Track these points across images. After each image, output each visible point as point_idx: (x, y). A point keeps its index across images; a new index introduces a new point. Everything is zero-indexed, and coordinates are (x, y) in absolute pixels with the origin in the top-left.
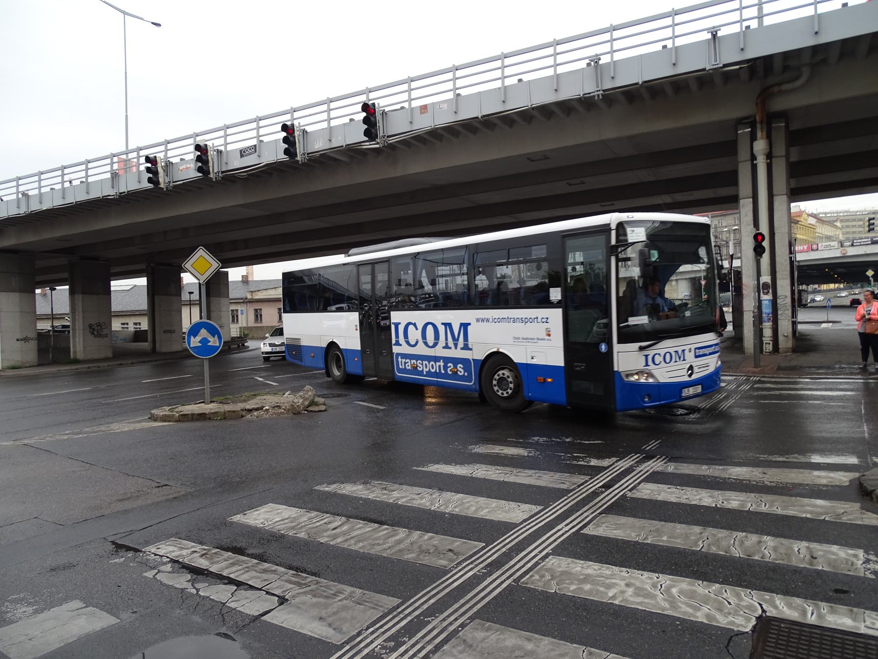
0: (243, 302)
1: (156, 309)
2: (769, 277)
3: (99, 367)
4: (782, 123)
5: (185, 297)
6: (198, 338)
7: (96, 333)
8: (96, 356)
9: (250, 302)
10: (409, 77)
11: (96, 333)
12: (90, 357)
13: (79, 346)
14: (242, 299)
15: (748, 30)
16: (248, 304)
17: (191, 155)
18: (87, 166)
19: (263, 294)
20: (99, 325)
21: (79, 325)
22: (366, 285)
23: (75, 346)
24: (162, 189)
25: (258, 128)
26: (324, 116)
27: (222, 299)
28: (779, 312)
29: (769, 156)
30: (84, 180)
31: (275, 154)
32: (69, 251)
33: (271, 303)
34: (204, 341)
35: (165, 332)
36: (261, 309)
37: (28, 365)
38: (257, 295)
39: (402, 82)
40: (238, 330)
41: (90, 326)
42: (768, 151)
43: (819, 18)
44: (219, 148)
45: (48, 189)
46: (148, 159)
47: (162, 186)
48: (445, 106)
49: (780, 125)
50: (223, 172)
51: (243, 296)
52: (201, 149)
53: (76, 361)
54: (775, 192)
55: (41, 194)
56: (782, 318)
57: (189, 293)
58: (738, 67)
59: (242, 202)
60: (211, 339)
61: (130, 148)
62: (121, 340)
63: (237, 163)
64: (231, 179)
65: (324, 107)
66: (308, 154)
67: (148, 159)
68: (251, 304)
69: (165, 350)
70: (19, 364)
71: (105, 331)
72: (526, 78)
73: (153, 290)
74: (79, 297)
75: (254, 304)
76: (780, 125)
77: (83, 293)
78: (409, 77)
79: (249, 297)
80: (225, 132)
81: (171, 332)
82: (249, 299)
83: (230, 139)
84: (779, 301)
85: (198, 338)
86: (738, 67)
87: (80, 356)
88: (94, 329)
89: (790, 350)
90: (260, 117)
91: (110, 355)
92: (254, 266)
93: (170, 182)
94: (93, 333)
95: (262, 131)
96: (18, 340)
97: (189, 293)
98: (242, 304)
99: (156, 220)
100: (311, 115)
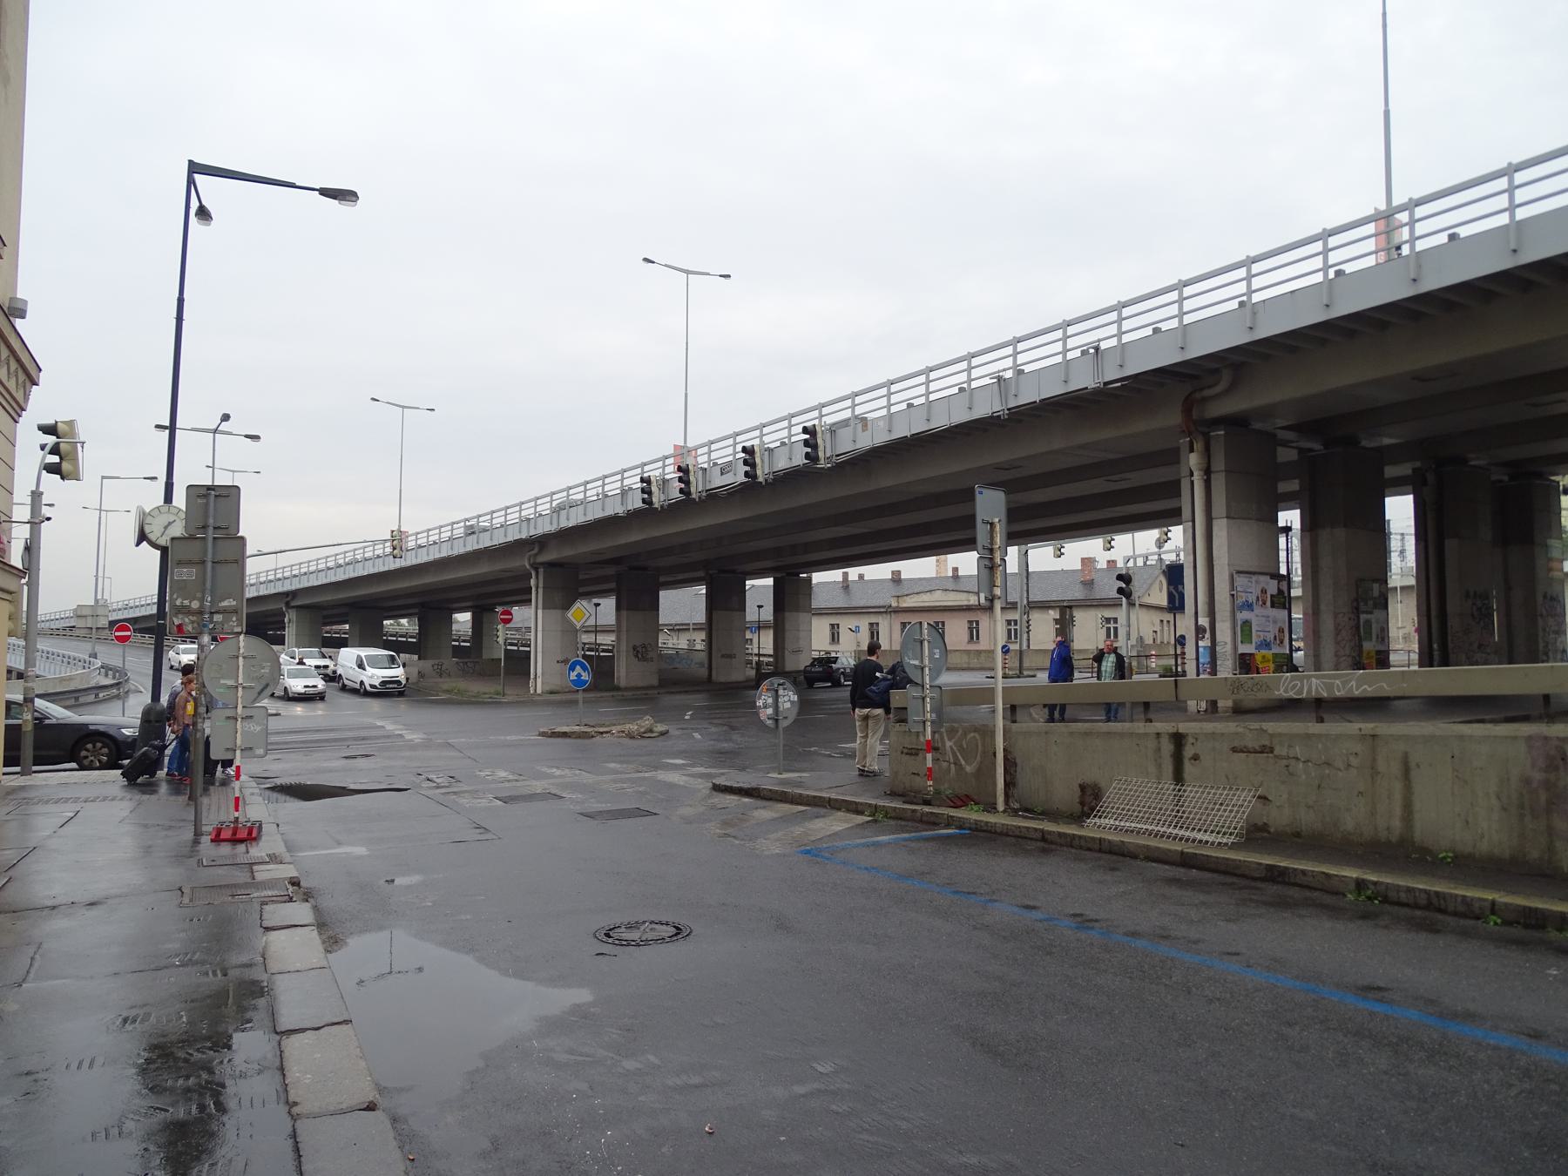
0: (886, 612)
1: (714, 627)
2: (1207, 619)
3: (623, 696)
4: (1221, 430)
5: (751, 614)
6: (575, 673)
7: (640, 656)
8: (641, 684)
9: (895, 612)
10: (1119, 302)
11: (640, 656)
12: (633, 684)
13: (624, 672)
14: (884, 607)
15: (1340, 278)
16: (892, 614)
17: (671, 473)
18: (603, 482)
19: (913, 600)
20: (644, 646)
21: (624, 647)
22: (1285, 568)
23: (619, 671)
24: (761, 483)
25: (1015, 354)
26: (1503, 201)
27: (801, 614)
28: (1218, 663)
29: (1208, 472)
30: (1244, 298)
31: (636, 502)
32: (616, 561)
33: (955, 614)
34: (579, 675)
35: (723, 656)
36: (877, 624)
37: (567, 690)
38: (905, 602)
39: (1362, 223)
40: (853, 654)
41: (635, 648)
42: (1206, 465)
43: (1519, 227)
44: (702, 466)
45: (1077, 353)
46: (744, 450)
47: (761, 479)
48: (881, 423)
49: (1219, 433)
50: (707, 491)
51: (887, 603)
52: (646, 480)
53: (618, 689)
54: (1214, 515)
55: (890, 416)
56: (1222, 669)
57: (758, 606)
58: (1119, 384)
59: (739, 517)
60: (583, 674)
61: (1395, 203)
62: (696, 664)
63: (718, 481)
64: (714, 498)
65: (1318, 246)
66: (774, 473)
67: (744, 450)
68: (897, 615)
69: (722, 679)
70: (558, 688)
71: (651, 655)
72: (1464, 232)
73: (712, 603)
74: (624, 613)
75: (900, 614)
76: (1219, 433)
77: (627, 609)
78: (1119, 302)
79: (894, 604)
80: (889, 390)
81: (731, 656)
82: (894, 608)
83: (1257, 283)
84: (1218, 648)
85: (575, 673)
86: (1119, 384)
87: (623, 684)
88: (638, 651)
89: (1230, 710)
90: (973, 353)
91: (655, 682)
92: (948, 556)
93: (665, 501)
94: (637, 656)
95: (1021, 359)
96: (558, 662)
97: (758, 606)
98: (884, 615)
99: (668, 535)
100: (776, 431)
